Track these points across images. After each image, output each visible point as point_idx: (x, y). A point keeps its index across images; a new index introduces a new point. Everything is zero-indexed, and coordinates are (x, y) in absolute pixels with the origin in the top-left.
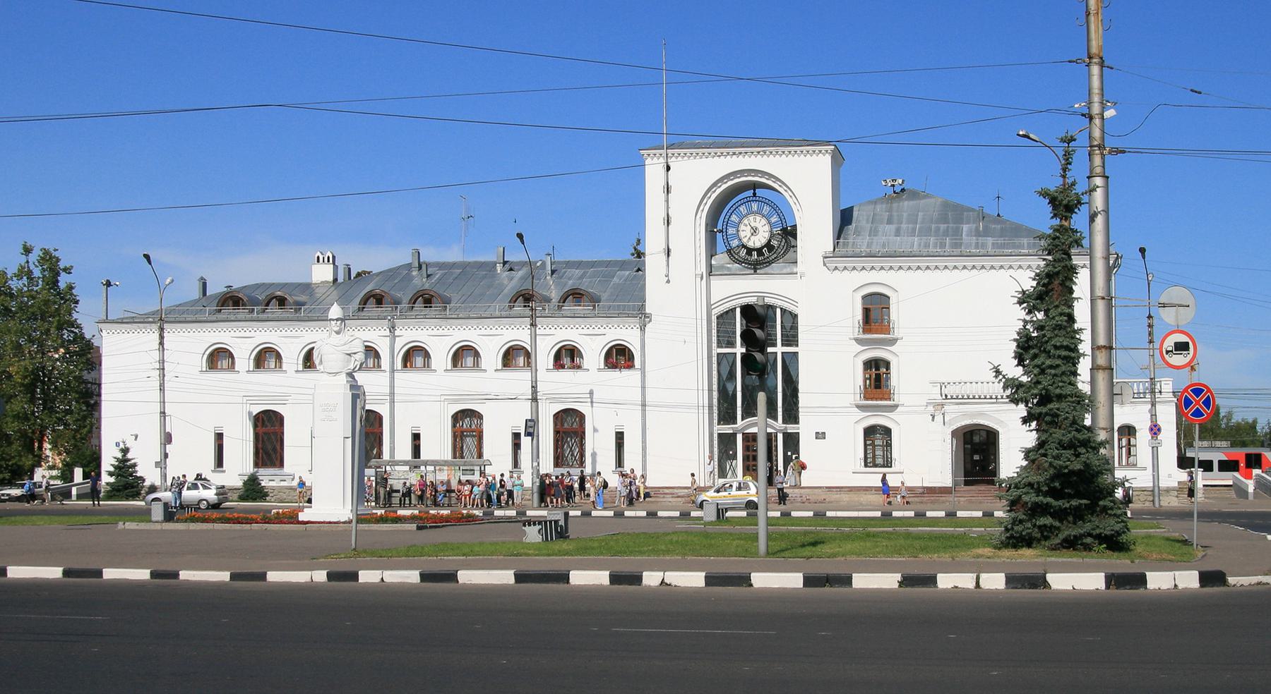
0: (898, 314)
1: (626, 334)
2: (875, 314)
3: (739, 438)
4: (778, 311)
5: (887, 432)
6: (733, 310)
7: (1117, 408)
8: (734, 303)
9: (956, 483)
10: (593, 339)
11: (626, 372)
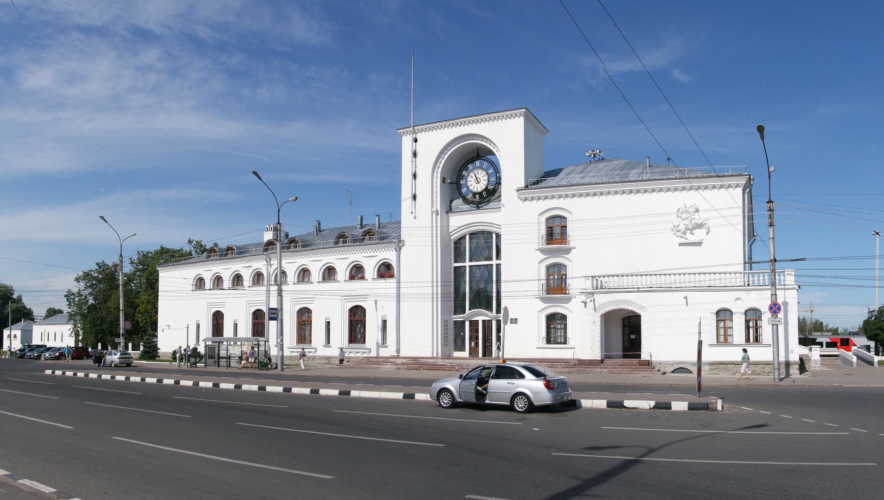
2: (556, 232)
3: (467, 324)
4: (494, 236)
5: (564, 317)
6: (464, 237)
8: (464, 231)
9: (607, 355)
10: (370, 258)
11: (389, 280)
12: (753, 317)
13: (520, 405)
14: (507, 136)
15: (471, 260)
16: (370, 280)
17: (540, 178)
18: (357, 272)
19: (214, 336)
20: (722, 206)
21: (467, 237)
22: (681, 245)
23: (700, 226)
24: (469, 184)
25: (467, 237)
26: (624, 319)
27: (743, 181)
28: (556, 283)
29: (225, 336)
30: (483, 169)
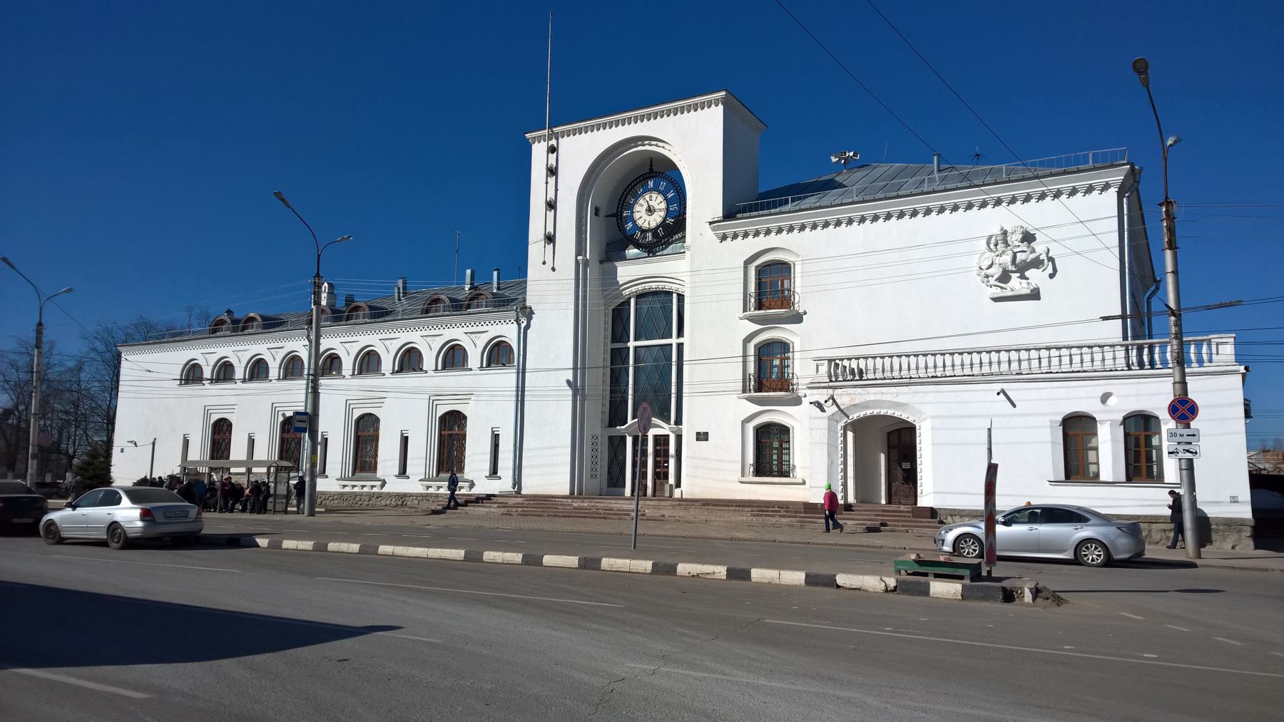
0: (802, 286)
1: (508, 331)
2: (771, 288)
6: (628, 302)
7: (322, 341)
10: (474, 335)
12: (1139, 430)
13: (1094, 555)
14: (694, 138)
15: (636, 340)
16: (388, 375)
17: (747, 199)
18: (453, 357)
19: (212, 458)
20: (1081, 225)
21: (633, 301)
22: (996, 300)
23: (1037, 263)
24: (636, 216)
25: (633, 301)
26: (889, 434)
27: (1117, 177)
28: (768, 372)
29: (232, 458)
30: (660, 192)
